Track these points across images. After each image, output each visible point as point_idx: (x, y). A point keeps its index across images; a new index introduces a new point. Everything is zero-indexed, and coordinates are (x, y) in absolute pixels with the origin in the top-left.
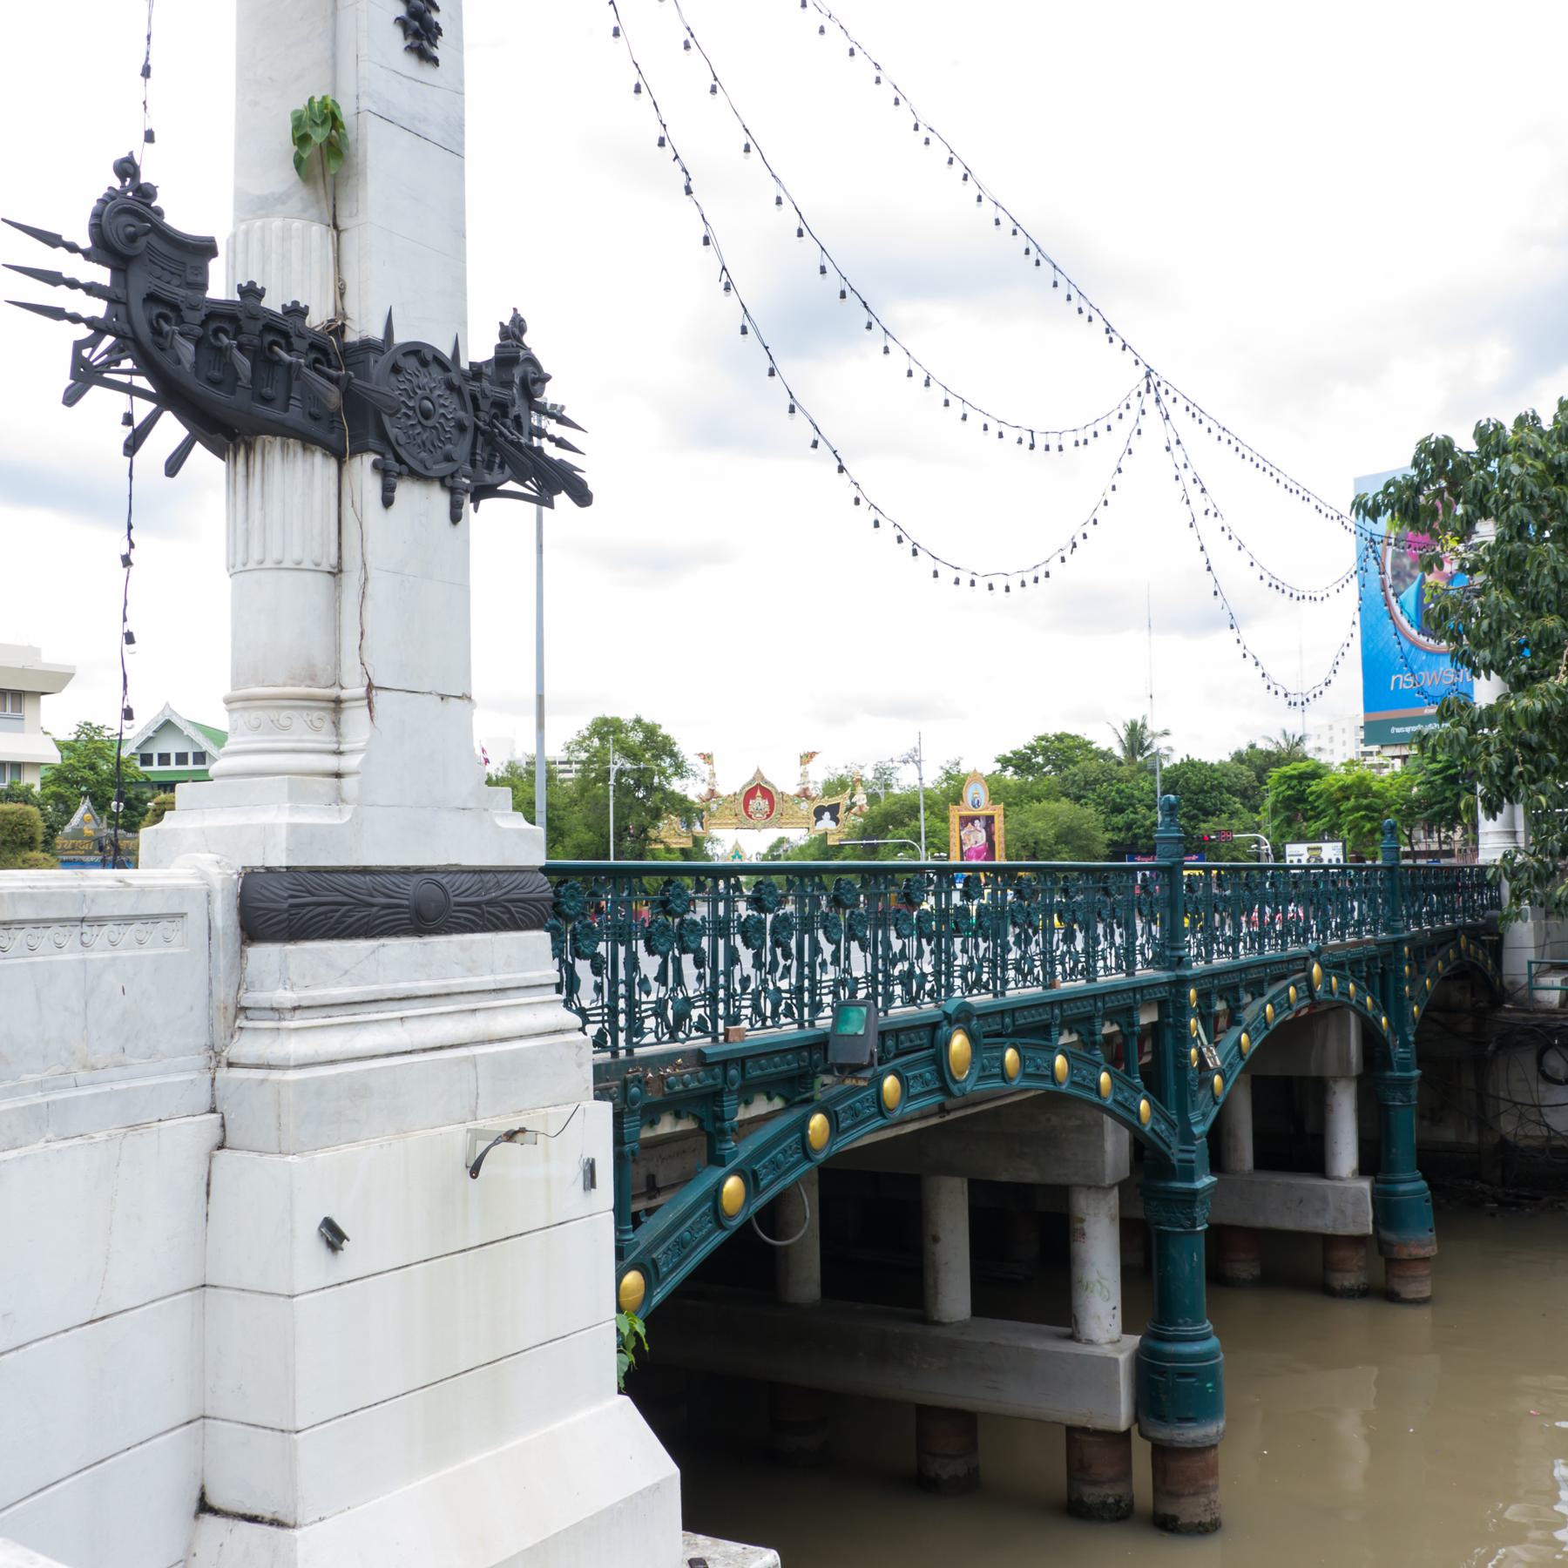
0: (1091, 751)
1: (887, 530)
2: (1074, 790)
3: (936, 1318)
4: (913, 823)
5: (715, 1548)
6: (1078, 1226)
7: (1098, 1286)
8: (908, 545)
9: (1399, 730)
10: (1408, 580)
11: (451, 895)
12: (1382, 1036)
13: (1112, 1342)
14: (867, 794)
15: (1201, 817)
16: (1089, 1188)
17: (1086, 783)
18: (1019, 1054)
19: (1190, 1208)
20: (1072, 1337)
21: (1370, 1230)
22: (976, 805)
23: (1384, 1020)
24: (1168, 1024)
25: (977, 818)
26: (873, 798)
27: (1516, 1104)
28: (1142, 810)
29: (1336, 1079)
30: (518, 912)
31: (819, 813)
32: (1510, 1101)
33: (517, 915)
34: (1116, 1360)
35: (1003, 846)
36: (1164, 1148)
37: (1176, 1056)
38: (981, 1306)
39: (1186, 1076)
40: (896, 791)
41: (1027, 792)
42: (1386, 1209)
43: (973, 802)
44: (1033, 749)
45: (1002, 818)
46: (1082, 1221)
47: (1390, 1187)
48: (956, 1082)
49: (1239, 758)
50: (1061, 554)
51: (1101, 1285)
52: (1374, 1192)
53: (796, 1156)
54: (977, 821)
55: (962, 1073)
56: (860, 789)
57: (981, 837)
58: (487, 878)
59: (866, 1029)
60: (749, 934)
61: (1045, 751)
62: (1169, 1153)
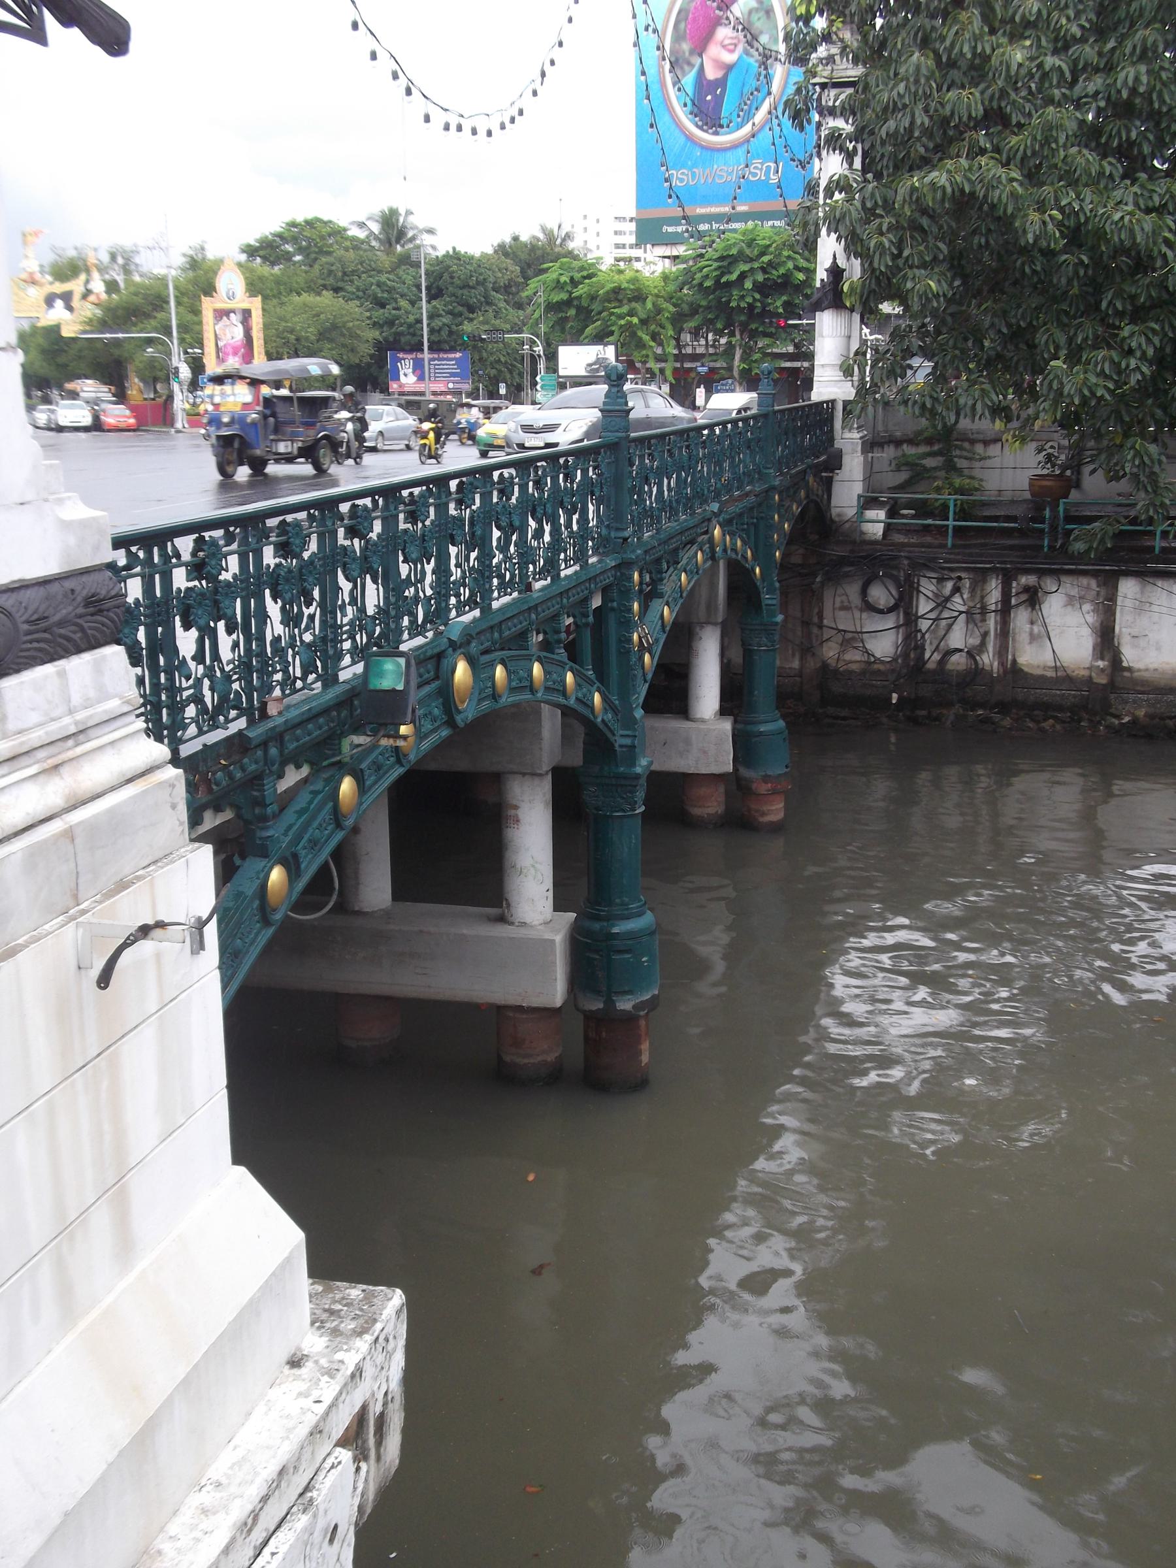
0: (347, 239)
1: (385, 64)
2: (331, 281)
3: (357, 909)
4: (160, 315)
5: (331, 1295)
6: (512, 812)
7: (532, 871)
8: (403, 82)
9: (670, 229)
10: (686, 68)
11: (20, 620)
12: (755, 584)
13: (546, 923)
14: (105, 281)
15: (467, 314)
16: (524, 774)
17: (345, 274)
18: (506, 667)
19: (630, 792)
20: (502, 919)
21: (730, 768)
22: (231, 297)
23: (758, 570)
24: (613, 609)
25: (233, 311)
26: (112, 286)
27: (840, 631)
28: (403, 303)
29: (702, 625)
30: (90, 628)
31: (50, 301)
32: (837, 629)
33: (89, 632)
34: (553, 941)
35: (262, 342)
36: (609, 735)
37: (620, 641)
38: (399, 894)
39: (629, 661)
40: (137, 278)
41: (285, 284)
42: (744, 744)
43: (227, 294)
44: (280, 236)
45: (260, 312)
46: (516, 807)
47: (749, 727)
48: (459, 712)
49: (502, 249)
50: (533, 86)
51: (536, 870)
52: (734, 730)
53: (330, 828)
54: (232, 315)
55: (463, 702)
56: (96, 275)
57: (238, 333)
58: (55, 588)
59: (407, 683)
60: (280, 588)
61: (294, 240)
62: (612, 739)
